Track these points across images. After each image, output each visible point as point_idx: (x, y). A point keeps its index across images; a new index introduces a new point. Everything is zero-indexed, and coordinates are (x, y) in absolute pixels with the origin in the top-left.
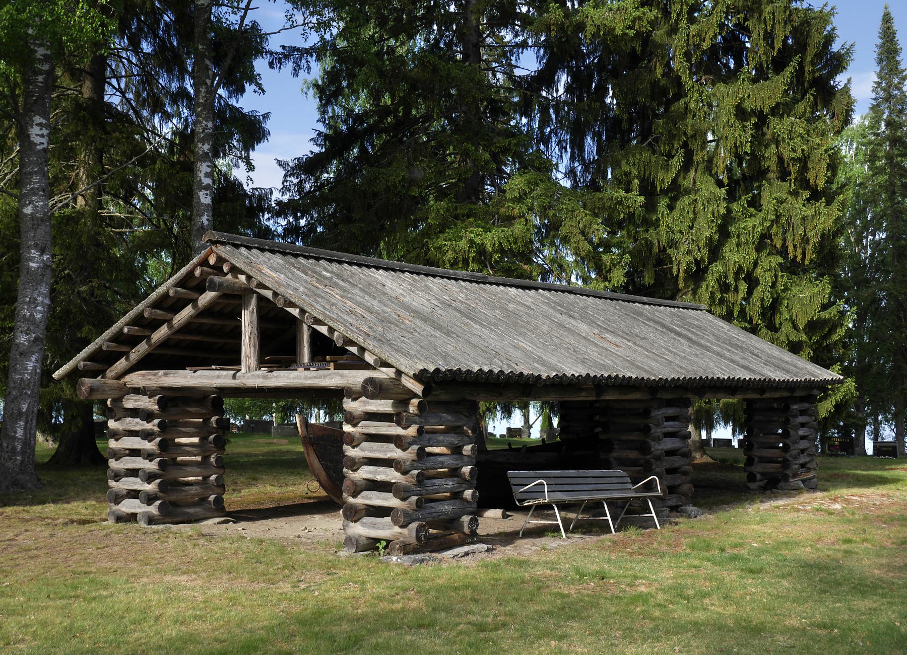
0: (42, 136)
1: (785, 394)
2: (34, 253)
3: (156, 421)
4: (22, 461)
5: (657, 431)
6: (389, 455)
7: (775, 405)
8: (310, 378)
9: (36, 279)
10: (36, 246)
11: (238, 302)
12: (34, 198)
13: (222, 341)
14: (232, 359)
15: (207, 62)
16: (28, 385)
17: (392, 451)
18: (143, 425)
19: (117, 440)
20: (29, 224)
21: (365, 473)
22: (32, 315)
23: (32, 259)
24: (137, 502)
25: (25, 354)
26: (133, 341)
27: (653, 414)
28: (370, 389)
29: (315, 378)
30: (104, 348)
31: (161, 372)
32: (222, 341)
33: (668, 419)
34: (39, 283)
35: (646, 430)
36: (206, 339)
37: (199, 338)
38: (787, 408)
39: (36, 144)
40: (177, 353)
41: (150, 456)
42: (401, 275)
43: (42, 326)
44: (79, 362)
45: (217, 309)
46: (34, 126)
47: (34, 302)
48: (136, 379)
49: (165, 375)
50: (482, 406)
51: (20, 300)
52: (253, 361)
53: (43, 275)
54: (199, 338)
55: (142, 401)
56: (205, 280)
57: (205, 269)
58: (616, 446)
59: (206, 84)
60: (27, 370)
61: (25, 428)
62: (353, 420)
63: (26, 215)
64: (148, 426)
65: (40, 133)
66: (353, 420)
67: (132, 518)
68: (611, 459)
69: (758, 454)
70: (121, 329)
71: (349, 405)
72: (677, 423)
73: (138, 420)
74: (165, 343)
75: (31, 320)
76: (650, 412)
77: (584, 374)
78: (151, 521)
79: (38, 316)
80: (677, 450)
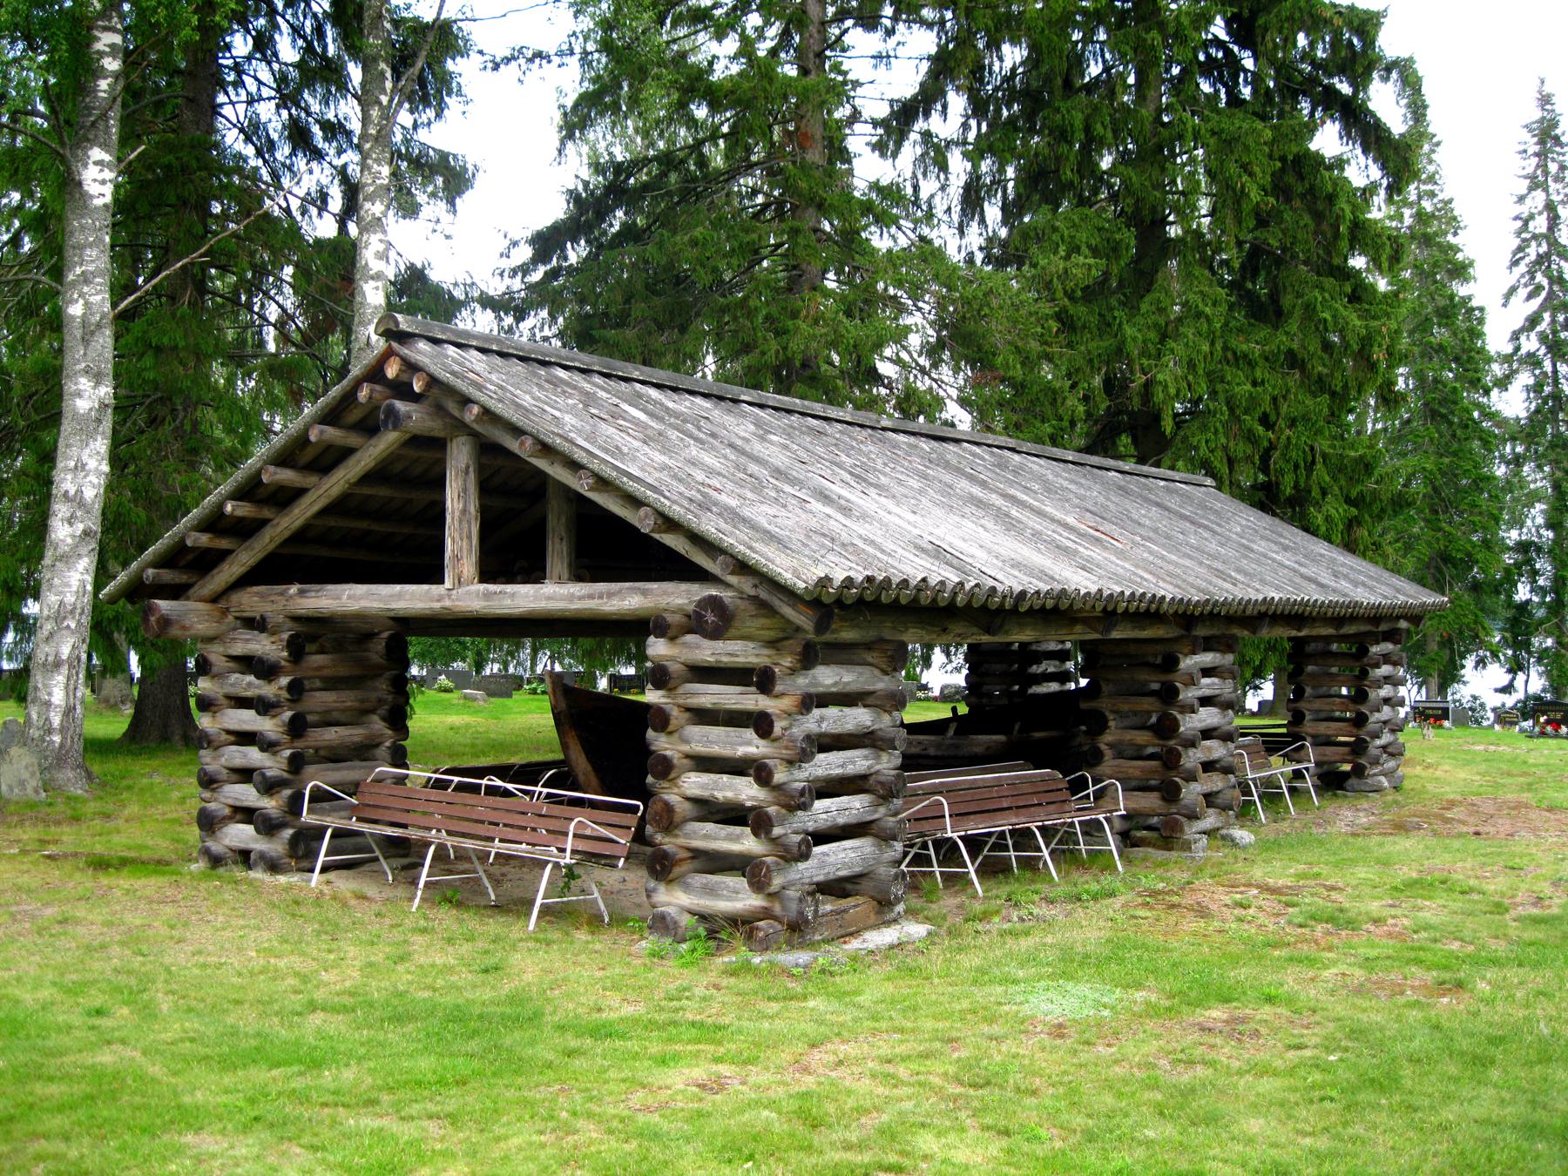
0: (103, 182)
1: (1364, 628)
2: (84, 383)
3: (284, 681)
4: (62, 745)
5: (1188, 694)
6: (741, 751)
7: (1334, 647)
8: (581, 598)
9: (88, 427)
10: (87, 371)
11: (439, 455)
12: (86, 289)
13: (406, 530)
14: (431, 572)
15: (383, 66)
16: (72, 612)
17: (749, 743)
18: (258, 687)
19: (1528, 389)
20: (78, 333)
21: (695, 783)
22: (79, 492)
23: (79, 394)
24: (249, 829)
25: (66, 559)
26: (245, 530)
27: (1182, 665)
28: (710, 617)
29: (591, 597)
30: (189, 543)
31: (293, 589)
32: (406, 530)
33: (1207, 672)
34: (91, 436)
35: (1169, 694)
36: (376, 527)
37: (363, 525)
38: (1364, 651)
39: (92, 197)
40: (325, 552)
41: (268, 746)
42: (239, 873)
43: (97, 508)
44: (142, 569)
45: (398, 467)
46: (91, 166)
47: (80, 467)
48: (252, 601)
49: (301, 593)
50: (916, 648)
51: (60, 464)
52: (469, 567)
53: (99, 421)
54: (363, 525)
55: (259, 642)
56: (377, 408)
57: (378, 387)
58: (1111, 724)
59: (380, 103)
60: (69, 586)
61: (67, 687)
62: (660, 677)
63: (73, 317)
64: (268, 690)
65: (100, 177)
66: (660, 677)
67: (244, 857)
68: (1103, 747)
69: (1310, 730)
70: (220, 506)
71: (657, 648)
72: (1215, 680)
73: (251, 678)
74: (299, 536)
75: (77, 500)
76: (1176, 662)
77: (1093, 589)
78: (274, 867)
79: (89, 494)
80: (1215, 729)
